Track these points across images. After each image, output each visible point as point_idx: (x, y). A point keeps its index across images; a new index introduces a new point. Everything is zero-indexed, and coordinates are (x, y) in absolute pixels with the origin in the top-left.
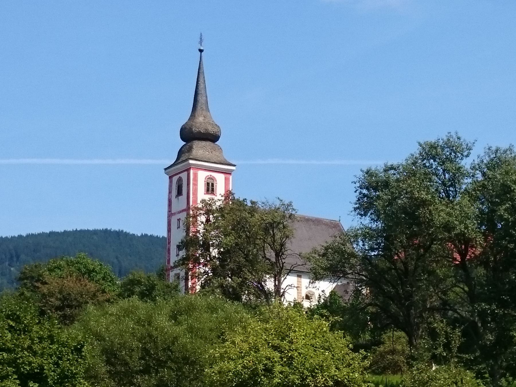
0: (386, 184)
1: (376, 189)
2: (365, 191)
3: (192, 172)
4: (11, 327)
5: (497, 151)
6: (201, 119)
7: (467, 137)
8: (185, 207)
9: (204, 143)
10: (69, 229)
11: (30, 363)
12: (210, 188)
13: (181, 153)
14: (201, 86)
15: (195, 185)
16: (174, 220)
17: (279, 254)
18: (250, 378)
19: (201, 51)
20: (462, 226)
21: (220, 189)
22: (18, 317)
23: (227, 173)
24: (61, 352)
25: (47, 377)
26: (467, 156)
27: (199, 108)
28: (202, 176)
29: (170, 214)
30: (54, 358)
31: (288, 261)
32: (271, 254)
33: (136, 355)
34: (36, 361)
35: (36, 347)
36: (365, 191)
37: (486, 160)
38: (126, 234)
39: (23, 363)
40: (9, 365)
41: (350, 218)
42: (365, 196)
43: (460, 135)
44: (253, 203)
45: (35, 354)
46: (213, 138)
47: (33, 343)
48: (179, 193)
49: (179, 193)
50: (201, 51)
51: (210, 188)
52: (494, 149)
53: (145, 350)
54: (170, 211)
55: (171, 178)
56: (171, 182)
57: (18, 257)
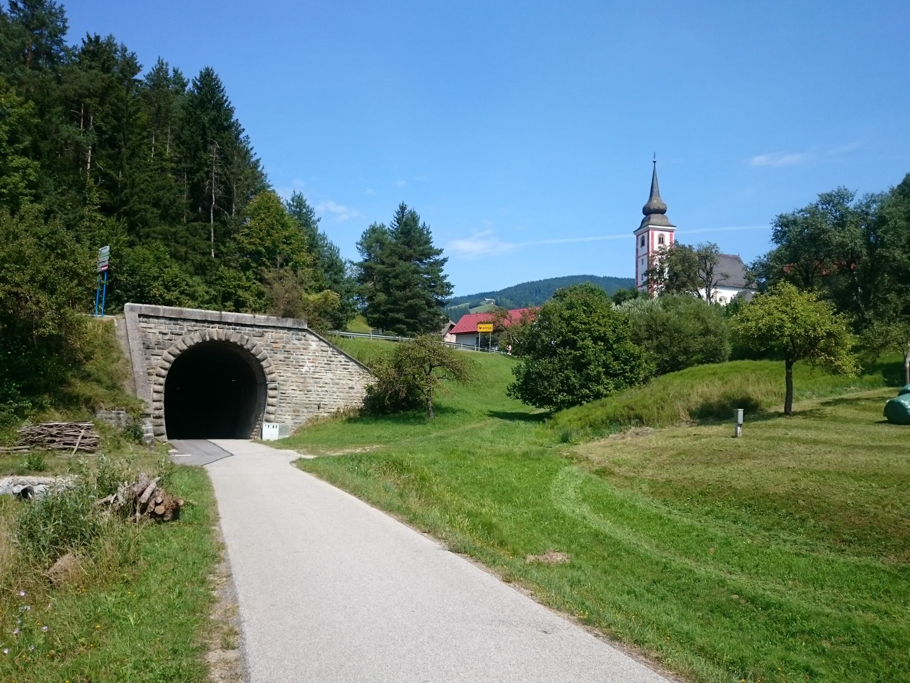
0: (795, 222)
1: (787, 226)
2: (779, 228)
3: (650, 232)
4: (584, 310)
5: (872, 196)
6: (655, 201)
7: (851, 189)
8: (646, 252)
9: (657, 215)
10: (565, 275)
11: (599, 331)
12: (661, 240)
13: (643, 222)
14: (655, 182)
15: (653, 239)
16: (640, 260)
17: (709, 274)
18: (768, 331)
19: (655, 162)
20: (853, 244)
21: (667, 242)
22: (588, 304)
23: (671, 231)
24: (615, 324)
25: (608, 339)
26: (852, 200)
27: (654, 195)
28: (656, 234)
29: (637, 257)
30: (612, 328)
31: (715, 278)
32: (704, 275)
33: (643, 328)
34: (602, 329)
35: (601, 321)
36: (779, 228)
37: (864, 202)
38: (595, 277)
39: (595, 330)
40: (586, 331)
41: (770, 245)
42: (778, 231)
43: (846, 187)
44: (690, 246)
45: (600, 325)
46: (662, 212)
47: (599, 319)
48: (643, 244)
49: (643, 244)
50: (655, 162)
51: (661, 240)
52: (870, 194)
53: (649, 326)
54: (637, 255)
55: (637, 236)
56: (637, 239)
57: (540, 291)
